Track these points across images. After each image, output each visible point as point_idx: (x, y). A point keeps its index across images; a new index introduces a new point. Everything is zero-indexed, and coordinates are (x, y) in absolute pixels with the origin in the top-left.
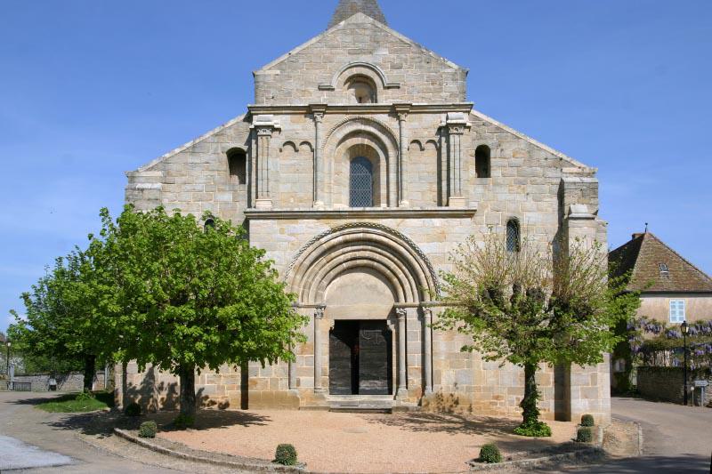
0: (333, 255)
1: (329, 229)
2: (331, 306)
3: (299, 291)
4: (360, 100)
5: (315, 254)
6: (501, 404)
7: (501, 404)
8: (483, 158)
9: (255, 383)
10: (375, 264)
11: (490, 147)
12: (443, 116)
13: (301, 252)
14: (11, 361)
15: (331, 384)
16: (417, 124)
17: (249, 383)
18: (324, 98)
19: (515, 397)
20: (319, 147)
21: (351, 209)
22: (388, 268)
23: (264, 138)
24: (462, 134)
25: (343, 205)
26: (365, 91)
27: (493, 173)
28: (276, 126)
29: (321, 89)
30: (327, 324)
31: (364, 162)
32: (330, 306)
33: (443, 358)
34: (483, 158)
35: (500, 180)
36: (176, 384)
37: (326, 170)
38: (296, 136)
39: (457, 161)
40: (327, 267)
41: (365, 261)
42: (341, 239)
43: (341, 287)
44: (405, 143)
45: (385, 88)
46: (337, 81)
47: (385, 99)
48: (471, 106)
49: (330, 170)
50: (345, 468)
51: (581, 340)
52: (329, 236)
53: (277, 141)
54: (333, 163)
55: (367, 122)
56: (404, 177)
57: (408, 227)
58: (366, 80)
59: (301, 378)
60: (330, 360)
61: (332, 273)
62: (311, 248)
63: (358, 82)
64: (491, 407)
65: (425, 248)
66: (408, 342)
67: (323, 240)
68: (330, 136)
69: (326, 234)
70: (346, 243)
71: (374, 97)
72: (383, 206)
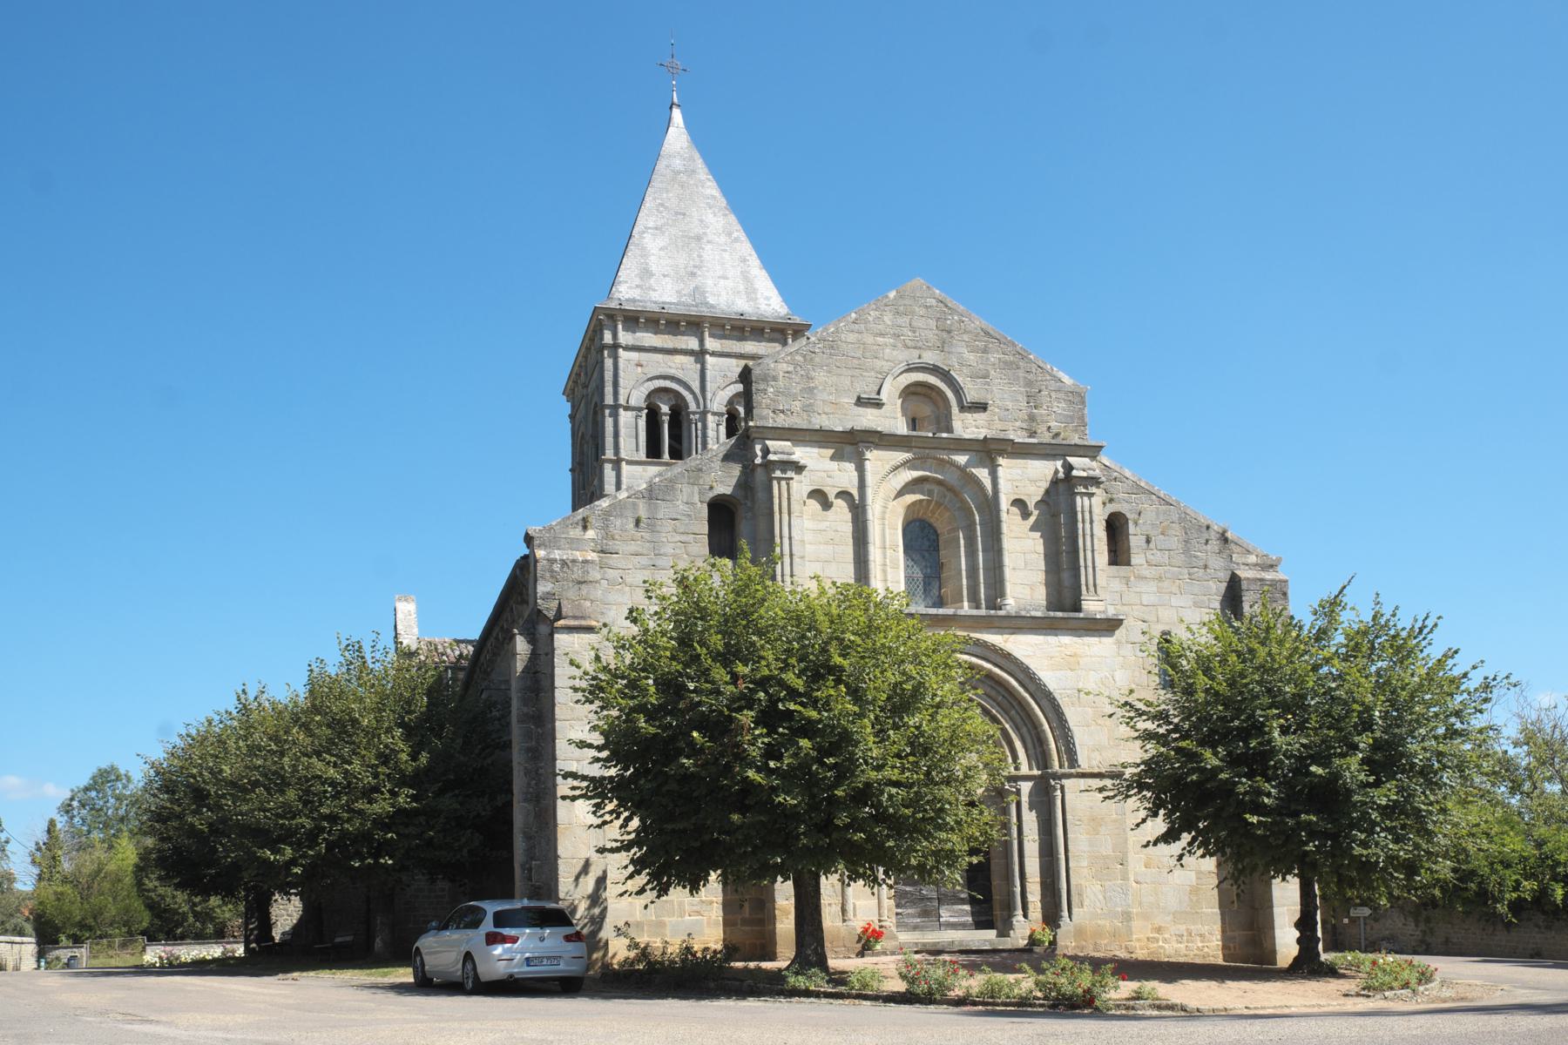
4: (913, 423)
6: (1165, 940)
7: (1165, 940)
8: (1116, 527)
12: (1059, 464)
14: (878, 461)
18: (868, 419)
20: (869, 500)
26: (925, 410)
29: (860, 402)
31: (922, 539)
33: (1085, 864)
34: (1116, 527)
35: (1146, 571)
36: (773, 958)
44: (1004, 503)
45: (962, 409)
47: (967, 426)
49: (884, 541)
50: (716, 923)
51: (609, 807)
53: (800, 486)
56: (1008, 560)
63: (914, 394)
65: (1050, 678)
68: (887, 482)
72: (966, 608)
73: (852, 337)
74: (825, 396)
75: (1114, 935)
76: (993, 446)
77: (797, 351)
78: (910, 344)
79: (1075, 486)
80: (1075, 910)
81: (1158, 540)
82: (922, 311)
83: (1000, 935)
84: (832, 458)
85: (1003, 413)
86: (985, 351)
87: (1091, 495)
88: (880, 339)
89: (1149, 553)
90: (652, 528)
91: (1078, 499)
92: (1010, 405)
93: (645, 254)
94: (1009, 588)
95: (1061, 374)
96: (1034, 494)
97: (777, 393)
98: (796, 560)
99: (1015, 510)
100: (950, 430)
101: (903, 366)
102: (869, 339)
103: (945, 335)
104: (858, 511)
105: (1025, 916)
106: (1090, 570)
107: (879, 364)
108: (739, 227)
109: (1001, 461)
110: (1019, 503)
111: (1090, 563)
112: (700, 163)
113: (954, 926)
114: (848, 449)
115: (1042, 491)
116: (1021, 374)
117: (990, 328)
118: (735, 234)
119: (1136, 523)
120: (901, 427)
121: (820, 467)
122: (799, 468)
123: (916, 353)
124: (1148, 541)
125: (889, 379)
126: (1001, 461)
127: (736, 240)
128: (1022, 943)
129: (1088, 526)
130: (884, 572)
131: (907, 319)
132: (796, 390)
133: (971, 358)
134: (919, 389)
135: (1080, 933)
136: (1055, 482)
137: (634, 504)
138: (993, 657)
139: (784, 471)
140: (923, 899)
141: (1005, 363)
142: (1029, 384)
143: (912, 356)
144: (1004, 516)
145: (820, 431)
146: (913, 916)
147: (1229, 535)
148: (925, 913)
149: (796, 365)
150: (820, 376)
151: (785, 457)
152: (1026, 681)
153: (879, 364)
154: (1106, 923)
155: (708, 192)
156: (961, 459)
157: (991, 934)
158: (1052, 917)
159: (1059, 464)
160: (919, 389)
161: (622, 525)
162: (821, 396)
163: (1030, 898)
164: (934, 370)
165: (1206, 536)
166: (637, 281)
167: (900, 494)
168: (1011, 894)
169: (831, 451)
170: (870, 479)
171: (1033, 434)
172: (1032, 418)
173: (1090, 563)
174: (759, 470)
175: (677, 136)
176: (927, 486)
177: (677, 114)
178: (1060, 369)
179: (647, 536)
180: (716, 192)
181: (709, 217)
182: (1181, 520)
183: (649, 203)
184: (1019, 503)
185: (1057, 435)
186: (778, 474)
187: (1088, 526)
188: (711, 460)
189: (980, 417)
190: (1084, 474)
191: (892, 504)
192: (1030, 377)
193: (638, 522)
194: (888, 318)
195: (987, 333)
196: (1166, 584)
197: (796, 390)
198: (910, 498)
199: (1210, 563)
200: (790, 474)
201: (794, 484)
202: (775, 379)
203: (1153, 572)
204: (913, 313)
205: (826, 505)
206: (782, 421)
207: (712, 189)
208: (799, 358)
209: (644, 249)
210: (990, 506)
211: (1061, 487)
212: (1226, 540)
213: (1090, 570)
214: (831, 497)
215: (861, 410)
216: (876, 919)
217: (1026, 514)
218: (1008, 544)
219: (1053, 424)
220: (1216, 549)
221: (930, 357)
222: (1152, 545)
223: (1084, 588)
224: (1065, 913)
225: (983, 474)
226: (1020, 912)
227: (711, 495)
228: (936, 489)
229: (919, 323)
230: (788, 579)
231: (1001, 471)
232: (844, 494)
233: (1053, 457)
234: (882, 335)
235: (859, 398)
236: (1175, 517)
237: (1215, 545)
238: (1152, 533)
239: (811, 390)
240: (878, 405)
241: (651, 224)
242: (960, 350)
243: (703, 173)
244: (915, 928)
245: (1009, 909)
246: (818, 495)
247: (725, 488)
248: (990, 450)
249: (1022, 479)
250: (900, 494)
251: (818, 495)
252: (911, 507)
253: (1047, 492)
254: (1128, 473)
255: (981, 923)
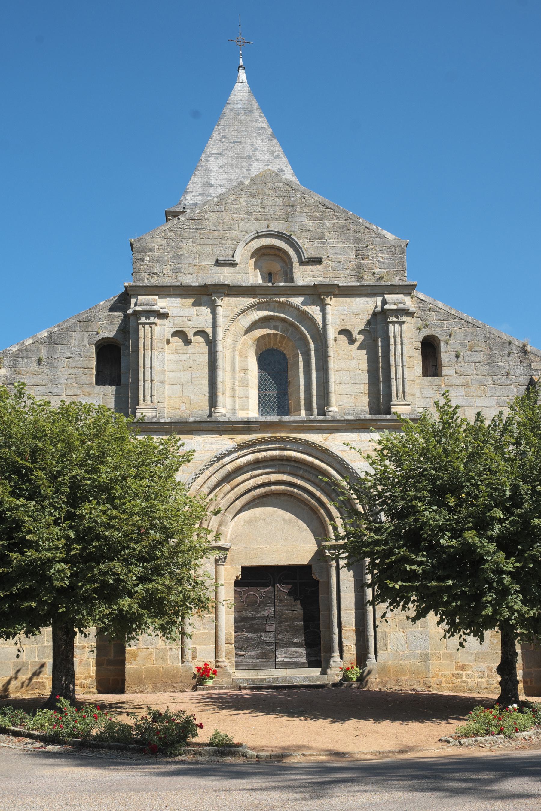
0: (240, 479)
1: (234, 445)
2: (235, 548)
3: (335, 374)
4: (269, 276)
5: (214, 480)
6: (468, 676)
7: (468, 676)
9: (135, 656)
10: (273, 488)
11: (440, 337)
12: (379, 300)
13: (197, 476)
14: (227, 306)
15: (237, 655)
16: (346, 308)
17: (126, 655)
18: (225, 276)
19: (486, 665)
20: (220, 336)
21: (263, 418)
22: (249, 490)
23: (147, 327)
24: (404, 322)
25: (252, 412)
26: (276, 266)
27: (445, 371)
28: (162, 311)
29: (218, 263)
30: (230, 573)
31: (274, 365)
32: (234, 548)
34: (430, 349)
35: (455, 380)
37: (228, 368)
38: (189, 324)
39: (399, 357)
40: (232, 495)
41: (278, 487)
42: (250, 457)
43: (250, 521)
44: (331, 333)
45: (302, 263)
46: (242, 254)
47: (304, 276)
48: (413, 287)
52: (235, 455)
53: (163, 329)
54: (237, 357)
55: (283, 307)
56: (332, 376)
57: (334, 443)
58: (277, 252)
59: (198, 648)
60: (236, 621)
61: (239, 504)
62: (211, 470)
63: (263, 255)
64: (455, 680)
66: (342, 594)
67: (227, 459)
68: (237, 331)
69: (229, 453)
70: (256, 464)
71: (289, 276)
73: (213, 216)
74: (190, 261)
75: (414, 672)
76: (320, 291)
77: (169, 229)
78: (260, 217)
79: (386, 317)
80: (380, 652)
81: (466, 355)
82: (271, 192)
83: (324, 672)
84: (194, 305)
85: (336, 265)
86: (322, 219)
87: (401, 323)
88: (236, 216)
89: (457, 366)
90: (51, 365)
91: (391, 327)
92: (342, 258)
93: (208, 171)
94: (333, 398)
95: (385, 232)
96: (357, 324)
97: (153, 260)
98: (155, 384)
99: (343, 337)
100: (292, 280)
101: (253, 234)
102: (228, 216)
103: (289, 209)
104: (212, 345)
105: (341, 657)
106: (400, 381)
107: (234, 234)
108: (280, 148)
109: (328, 300)
110: (345, 332)
111: (400, 376)
112: (256, 105)
113: (286, 665)
114: (205, 299)
115: (364, 322)
116: (351, 233)
117: (326, 202)
118: (276, 153)
119: (447, 343)
120: (255, 278)
121: (182, 312)
122: (164, 316)
123: (265, 224)
124: (457, 357)
125: (242, 244)
126: (328, 300)
127: (277, 157)
128: (337, 679)
129: (399, 347)
130: (233, 390)
131: (258, 199)
132: (167, 257)
133: (310, 224)
134: (269, 251)
135: (384, 671)
136: (375, 315)
137: (37, 348)
138: (314, 452)
139: (148, 318)
140: (263, 643)
141: (339, 226)
142: (358, 241)
143: (262, 227)
144: (331, 343)
145: (181, 287)
146: (254, 657)
147: (528, 348)
148: (264, 655)
149: (168, 239)
150: (187, 247)
151: (147, 308)
152: (342, 471)
153: (234, 234)
154: (406, 663)
155: (260, 125)
156: (297, 301)
157: (316, 672)
158: (362, 658)
159: (379, 300)
160: (269, 251)
161: (27, 364)
162: (186, 261)
163: (345, 642)
164: (279, 236)
165: (508, 350)
166: (200, 191)
167: (249, 330)
168: (331, 640)
169: (192, 300)
170: (220, 320)
171: (360, 279)
172: (359, 267)
173: (400, 376)
174: (132, 318)
175: (241, 88)
176: (273, 323)
177: (242, 75)
178: (384, 228)
179: (46, 371)
180: (265, 125)
181: (259, 143)
182: (486, 339)
183: (216, 135)
184: (345, 332)
185: (381, 278)
186: (143, 320)
187: (399, 347)
188: (98, 313)
189: (316, 268)
190: (395, 307)
191: (241, 340)
192: (360, 235)
193: (39, 361)
194: (243, 200)
195: (324, 205)
196: (472, 390)
197: (167, 257)
198: (259, 333)
199: (511, 371)
200: (152, 320)
201: (156, 329)
202: (151, 250)
203: (462, 380)
204: (264, 194)
205: (187, 342)
206: (155, 281)
207: (263, 123)
208: (171, 234)
209: (207, 168)
210: (321, 337)
211: (379, 317)
212: (526, 352)
213: (400, 381)
214: (191, 336)
215: (219, 269)
216: (213, 660)
217: (352, 341)
218: (334, 363)
219: (377, 271)
220: (517, 359)
221: (275, 227)
222: (461, 359)
223: (394, 396)
224: (372, 655)
225: (314, 311)
226: (337, 653)
227: (97, 338)
228: (280, 325)
229: (268, 201)
230: (148, 399)
231: (329, 309)
232: (200, 333)
233: (375, 295)
234: (238, 212)
235: (217, 260)
236: (481, 337)
237: (516, 356)
238: (460, 350)
239: (179, 257)
240: (233, 264)
241: (215, 151)
242: (301, 219)
243: (257, 113)
244: (255, 667)
245: (330, 651)
246: (180, 334)
247: (109, 332)
248: (318, 294)
249: (347, 314)
250: (249, 330)
251: (180, 334)
252: (260, 340)
253: (369, 323)
254: (440, 304)
255: (313, 663)
